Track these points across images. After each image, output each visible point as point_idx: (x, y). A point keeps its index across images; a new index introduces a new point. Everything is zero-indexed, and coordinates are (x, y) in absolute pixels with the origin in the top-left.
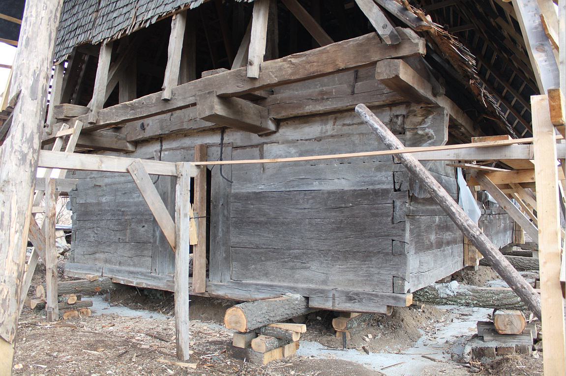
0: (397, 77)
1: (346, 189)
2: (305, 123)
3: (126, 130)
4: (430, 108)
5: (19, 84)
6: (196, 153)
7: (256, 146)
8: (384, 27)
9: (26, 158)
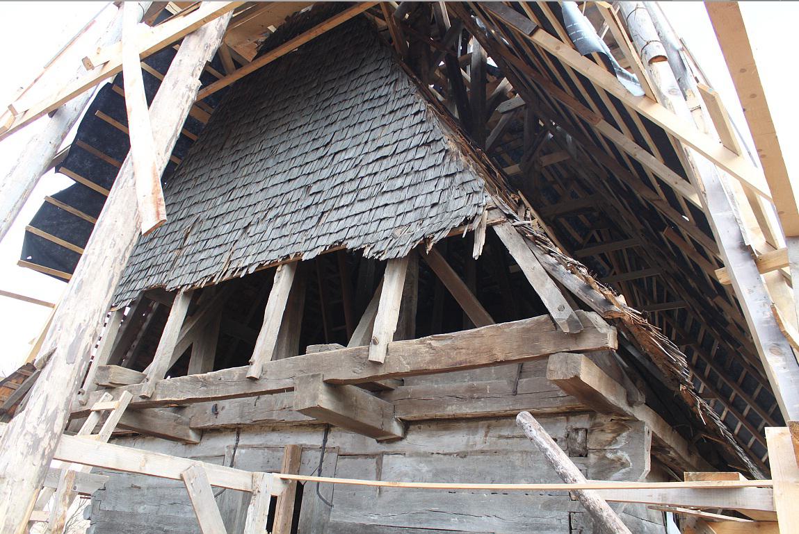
0: (577, 378)
2: (446, 429)
3: (190, 412)
4: (623, 422)
5: (56, 340)
6: (286, 458)
7: (373, 456)
8: (561, 309)
9: (38, 445)
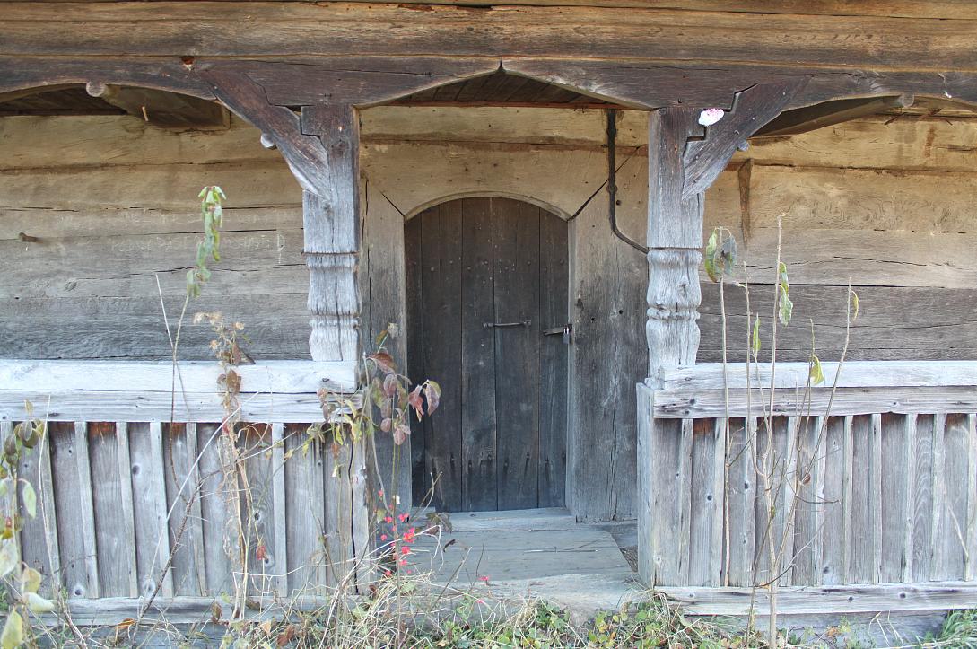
1: (950, 286)
